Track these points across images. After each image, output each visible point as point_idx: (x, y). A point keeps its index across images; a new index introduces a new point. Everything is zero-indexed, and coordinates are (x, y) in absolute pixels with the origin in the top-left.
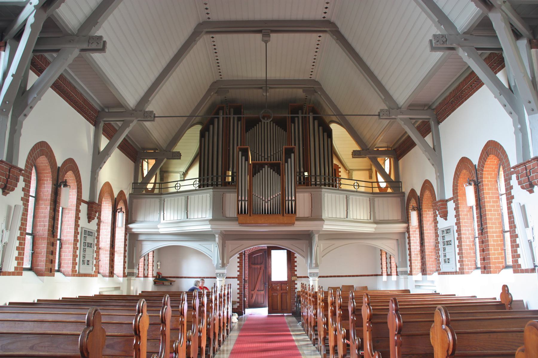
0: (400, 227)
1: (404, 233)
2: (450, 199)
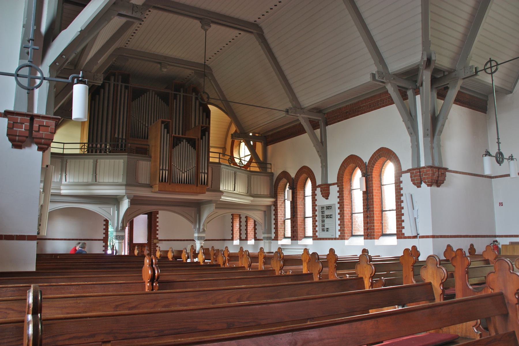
0: (269, 201)
1: (269, 207)
2: (334, 184)
